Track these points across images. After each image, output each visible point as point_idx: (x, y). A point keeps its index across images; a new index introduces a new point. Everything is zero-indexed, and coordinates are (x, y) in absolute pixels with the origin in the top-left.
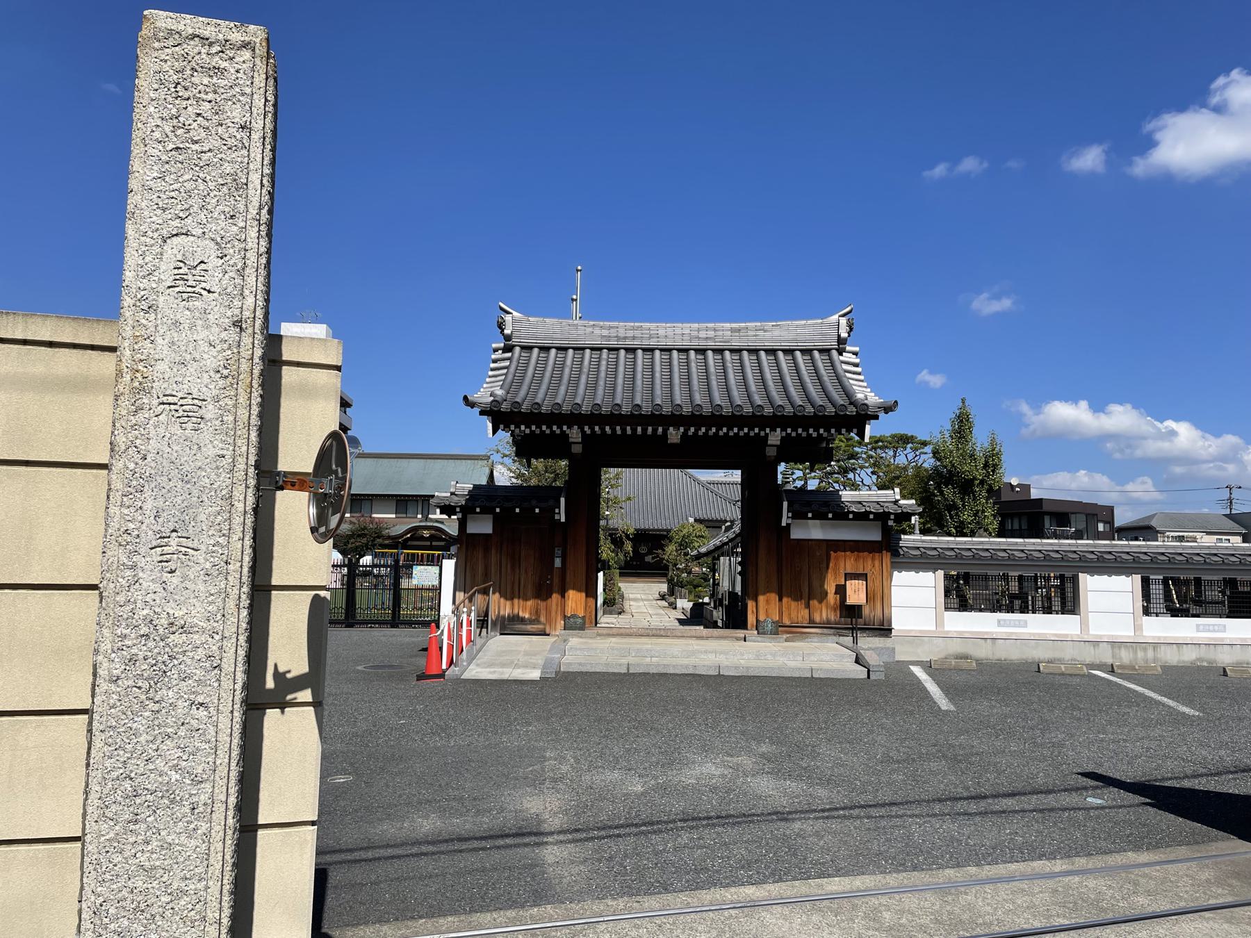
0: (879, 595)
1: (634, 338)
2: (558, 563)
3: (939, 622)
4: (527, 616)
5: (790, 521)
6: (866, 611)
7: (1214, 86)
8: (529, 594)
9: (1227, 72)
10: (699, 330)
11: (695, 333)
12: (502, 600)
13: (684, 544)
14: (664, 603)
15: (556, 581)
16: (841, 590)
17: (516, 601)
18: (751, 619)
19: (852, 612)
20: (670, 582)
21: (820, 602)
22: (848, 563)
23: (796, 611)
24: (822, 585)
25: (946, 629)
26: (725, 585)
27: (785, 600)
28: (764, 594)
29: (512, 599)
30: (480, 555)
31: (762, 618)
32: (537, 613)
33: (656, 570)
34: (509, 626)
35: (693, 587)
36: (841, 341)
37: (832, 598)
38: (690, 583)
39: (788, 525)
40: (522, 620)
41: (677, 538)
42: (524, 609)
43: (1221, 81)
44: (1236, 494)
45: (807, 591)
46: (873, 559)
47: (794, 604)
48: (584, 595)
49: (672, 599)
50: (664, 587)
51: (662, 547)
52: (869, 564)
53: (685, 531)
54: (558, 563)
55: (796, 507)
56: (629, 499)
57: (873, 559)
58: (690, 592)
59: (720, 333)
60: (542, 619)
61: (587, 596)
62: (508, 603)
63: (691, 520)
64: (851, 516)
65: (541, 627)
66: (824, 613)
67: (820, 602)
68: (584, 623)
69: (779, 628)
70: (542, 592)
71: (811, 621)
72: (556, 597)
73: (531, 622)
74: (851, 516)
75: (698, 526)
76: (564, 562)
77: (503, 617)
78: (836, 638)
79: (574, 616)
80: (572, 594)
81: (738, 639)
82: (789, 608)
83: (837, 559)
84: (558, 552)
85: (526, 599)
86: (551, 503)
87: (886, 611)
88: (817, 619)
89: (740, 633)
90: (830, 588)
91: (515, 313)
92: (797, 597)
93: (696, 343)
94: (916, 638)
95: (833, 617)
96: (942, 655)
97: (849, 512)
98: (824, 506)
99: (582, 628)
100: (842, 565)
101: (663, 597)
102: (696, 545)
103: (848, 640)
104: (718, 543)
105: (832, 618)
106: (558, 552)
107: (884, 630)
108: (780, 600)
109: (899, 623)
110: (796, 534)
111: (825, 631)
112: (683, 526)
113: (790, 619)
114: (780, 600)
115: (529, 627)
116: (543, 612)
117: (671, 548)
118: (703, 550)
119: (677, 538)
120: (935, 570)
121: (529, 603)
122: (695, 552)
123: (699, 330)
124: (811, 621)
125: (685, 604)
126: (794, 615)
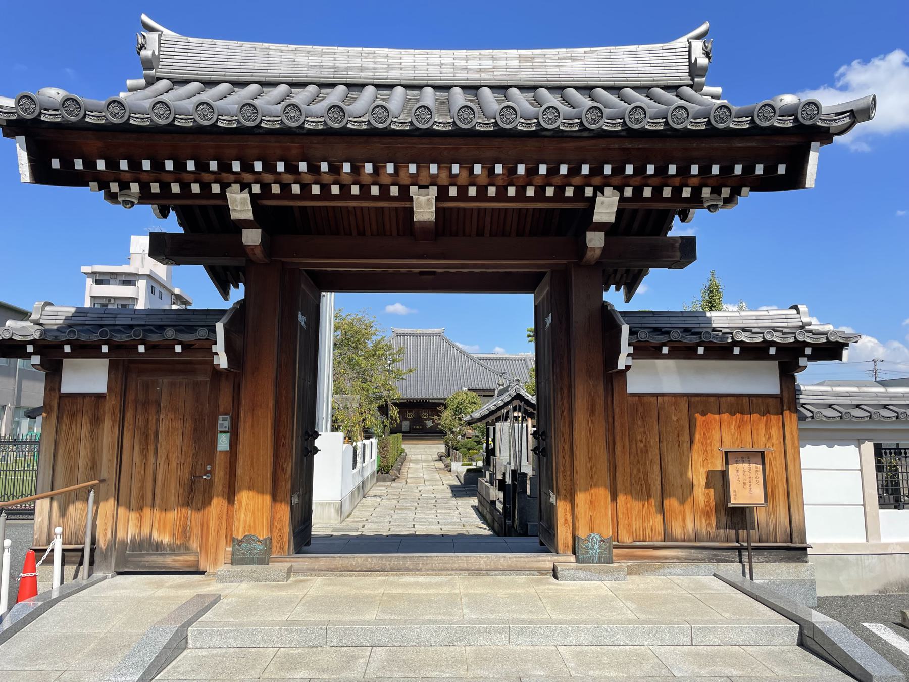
0: (785, 488)
1: (362, 69)
2: (223, 442)
3: (870, 528)
4: (166, 539)
5: (630, 361)
6: (760, 517)
7: (837, 75)
8: (173, 499)
9: (849, 63)
10: (467, 59)
11: (462, 63)
12: (122, 510)
13: (458, 411)
14: (441, 465)
15: (220, 475)
16: (720, 481)
17: (147, 512)
18: (563, 534)
19: (738, 517)
20: (447, 444)
21: (682, 502)
22: (723, 433)
23: (640, 518)
24: (683, 473)
25: (884, 540)
26: (504, 458)
27: (621, 499)
28: (587, 489)
29: (141, 509)
30: (85, 429)
31: (582, 533)
32: (185, 533)
33: (436, 433)
34: (135, 560)
35: (468, 452)
36: (694, 70)
37: (702, 495)
38: (463, 446)
39: (628, 367)
40: (158, 548)
41: (453, 405)
42: (159, 526)
43: (843, 69)
44: (879, 366)
45: (656, 484)
46: (768, 426)
47: (636, 506)
48: (268, 498)
49: (448, 461)
50: (442, 448)
51: (438, 413)
52: (762, 433)
53: (459, 399)
54: (223, 442)
55: (643, 335)
56: (410, 371)
57: (768, 426)
58: (464, 455)
59: (502, 63)
60: (194, 545)
61: (275, 499)
62: (133, 516)
63: (465, 389)
64: (737, 351)
65: (190, 558)
66: (691, 520)
67: (682, 502)
68: (269, 550)
69: (618, 550)
70: (195, 494)
71: (668, 536)
72: (218, 503)
73: (174, 550)
74: (737, 351)
75: (470, 393)
76: (234, 442)
77: (123, 543)
78: (713, 567)
79: (248, 539)
80: (245, 497)
81: (541, 572)
82: (628, 515)
83: (707, 426)
84: (224, 423)
85: (165, 509)
86: (202, 333)
87: (795, 517)
88: (678, 532)
89: (546, 560)
90: (699, 478)
91: (166, 31)
92: (643, 493)
93: (462, 77)
94: (839, 557)
95: (706, 527)
96: (878, 585)
97: (735, 343)
98: (686, 340)
99: (263, 560)
100: (716, 436)
101: (440, 459)
102: (469, 410)
103: (733, 569)
104: (493, 408)
105: (704, 530)
106: (224, 423)
107: (795, 549)
108: (614, 498)
109: (816, 536)
110: (636, 384)
111: (694, 553)
112: (457, 394)
113: (631, 532)
114: (614, 498)
115: (169, 561)
116: (196, 531)
117: (447, 414)
118: (477, 415)
119: (453, 405)
120: (859, 443)
121: (172, 515)
122: (468, 418)
123: (467, 59)
124: (668, 536)
125: (460, 468)
126: (637, 525)
